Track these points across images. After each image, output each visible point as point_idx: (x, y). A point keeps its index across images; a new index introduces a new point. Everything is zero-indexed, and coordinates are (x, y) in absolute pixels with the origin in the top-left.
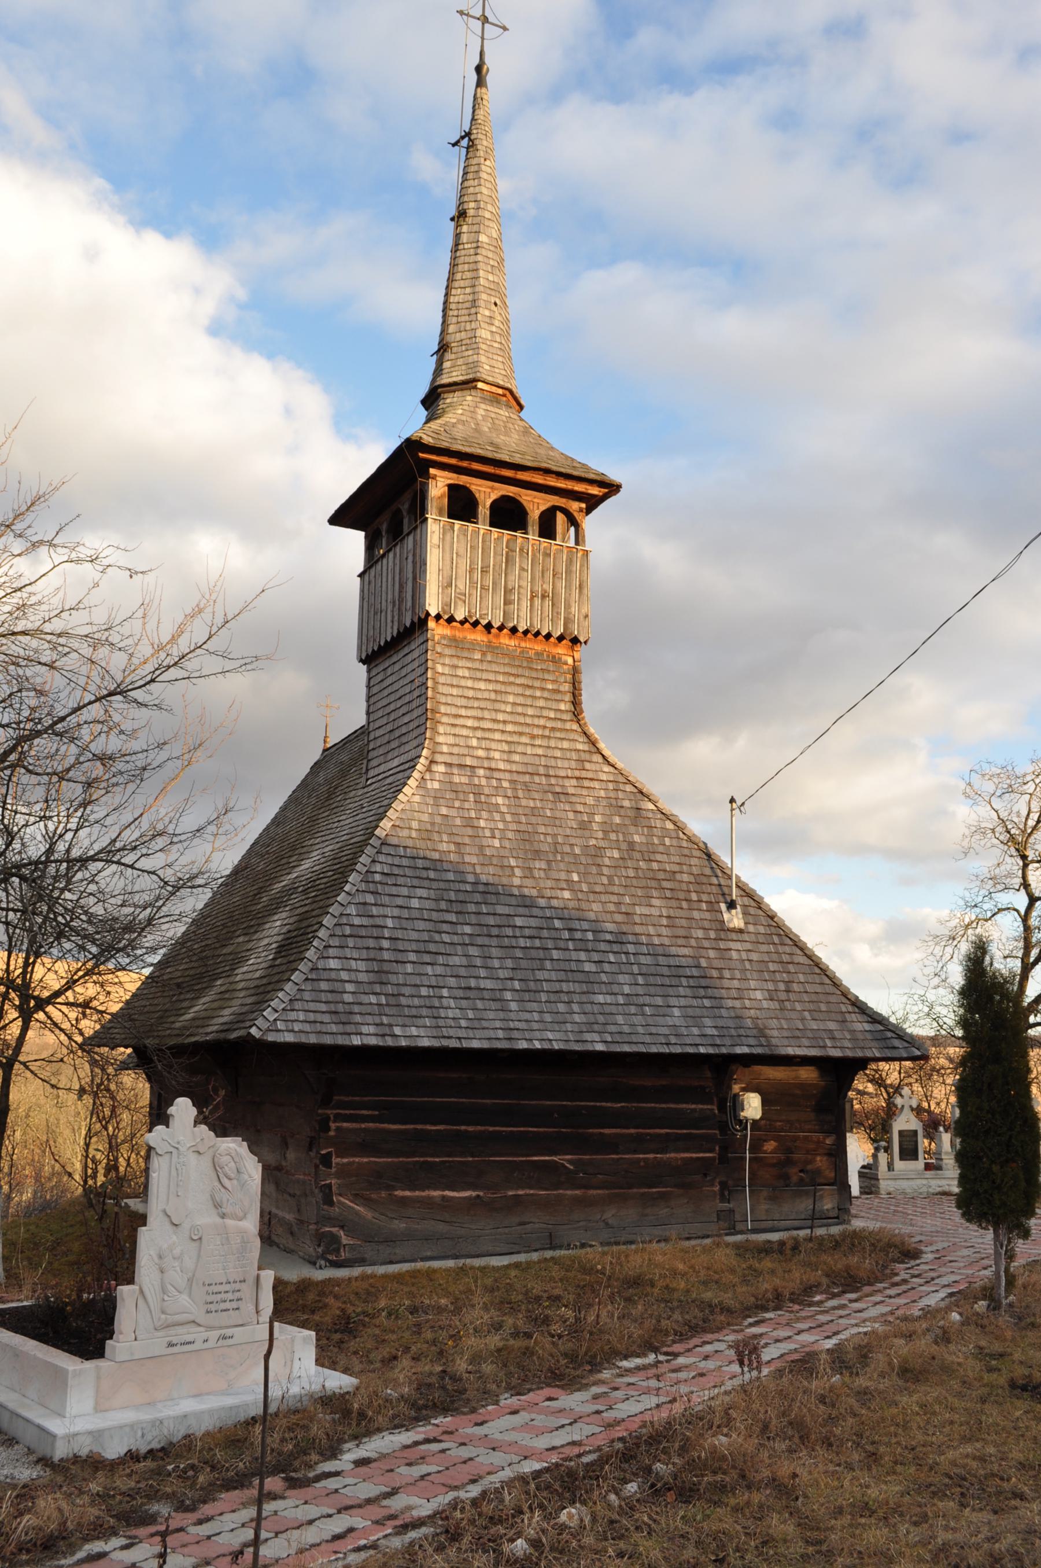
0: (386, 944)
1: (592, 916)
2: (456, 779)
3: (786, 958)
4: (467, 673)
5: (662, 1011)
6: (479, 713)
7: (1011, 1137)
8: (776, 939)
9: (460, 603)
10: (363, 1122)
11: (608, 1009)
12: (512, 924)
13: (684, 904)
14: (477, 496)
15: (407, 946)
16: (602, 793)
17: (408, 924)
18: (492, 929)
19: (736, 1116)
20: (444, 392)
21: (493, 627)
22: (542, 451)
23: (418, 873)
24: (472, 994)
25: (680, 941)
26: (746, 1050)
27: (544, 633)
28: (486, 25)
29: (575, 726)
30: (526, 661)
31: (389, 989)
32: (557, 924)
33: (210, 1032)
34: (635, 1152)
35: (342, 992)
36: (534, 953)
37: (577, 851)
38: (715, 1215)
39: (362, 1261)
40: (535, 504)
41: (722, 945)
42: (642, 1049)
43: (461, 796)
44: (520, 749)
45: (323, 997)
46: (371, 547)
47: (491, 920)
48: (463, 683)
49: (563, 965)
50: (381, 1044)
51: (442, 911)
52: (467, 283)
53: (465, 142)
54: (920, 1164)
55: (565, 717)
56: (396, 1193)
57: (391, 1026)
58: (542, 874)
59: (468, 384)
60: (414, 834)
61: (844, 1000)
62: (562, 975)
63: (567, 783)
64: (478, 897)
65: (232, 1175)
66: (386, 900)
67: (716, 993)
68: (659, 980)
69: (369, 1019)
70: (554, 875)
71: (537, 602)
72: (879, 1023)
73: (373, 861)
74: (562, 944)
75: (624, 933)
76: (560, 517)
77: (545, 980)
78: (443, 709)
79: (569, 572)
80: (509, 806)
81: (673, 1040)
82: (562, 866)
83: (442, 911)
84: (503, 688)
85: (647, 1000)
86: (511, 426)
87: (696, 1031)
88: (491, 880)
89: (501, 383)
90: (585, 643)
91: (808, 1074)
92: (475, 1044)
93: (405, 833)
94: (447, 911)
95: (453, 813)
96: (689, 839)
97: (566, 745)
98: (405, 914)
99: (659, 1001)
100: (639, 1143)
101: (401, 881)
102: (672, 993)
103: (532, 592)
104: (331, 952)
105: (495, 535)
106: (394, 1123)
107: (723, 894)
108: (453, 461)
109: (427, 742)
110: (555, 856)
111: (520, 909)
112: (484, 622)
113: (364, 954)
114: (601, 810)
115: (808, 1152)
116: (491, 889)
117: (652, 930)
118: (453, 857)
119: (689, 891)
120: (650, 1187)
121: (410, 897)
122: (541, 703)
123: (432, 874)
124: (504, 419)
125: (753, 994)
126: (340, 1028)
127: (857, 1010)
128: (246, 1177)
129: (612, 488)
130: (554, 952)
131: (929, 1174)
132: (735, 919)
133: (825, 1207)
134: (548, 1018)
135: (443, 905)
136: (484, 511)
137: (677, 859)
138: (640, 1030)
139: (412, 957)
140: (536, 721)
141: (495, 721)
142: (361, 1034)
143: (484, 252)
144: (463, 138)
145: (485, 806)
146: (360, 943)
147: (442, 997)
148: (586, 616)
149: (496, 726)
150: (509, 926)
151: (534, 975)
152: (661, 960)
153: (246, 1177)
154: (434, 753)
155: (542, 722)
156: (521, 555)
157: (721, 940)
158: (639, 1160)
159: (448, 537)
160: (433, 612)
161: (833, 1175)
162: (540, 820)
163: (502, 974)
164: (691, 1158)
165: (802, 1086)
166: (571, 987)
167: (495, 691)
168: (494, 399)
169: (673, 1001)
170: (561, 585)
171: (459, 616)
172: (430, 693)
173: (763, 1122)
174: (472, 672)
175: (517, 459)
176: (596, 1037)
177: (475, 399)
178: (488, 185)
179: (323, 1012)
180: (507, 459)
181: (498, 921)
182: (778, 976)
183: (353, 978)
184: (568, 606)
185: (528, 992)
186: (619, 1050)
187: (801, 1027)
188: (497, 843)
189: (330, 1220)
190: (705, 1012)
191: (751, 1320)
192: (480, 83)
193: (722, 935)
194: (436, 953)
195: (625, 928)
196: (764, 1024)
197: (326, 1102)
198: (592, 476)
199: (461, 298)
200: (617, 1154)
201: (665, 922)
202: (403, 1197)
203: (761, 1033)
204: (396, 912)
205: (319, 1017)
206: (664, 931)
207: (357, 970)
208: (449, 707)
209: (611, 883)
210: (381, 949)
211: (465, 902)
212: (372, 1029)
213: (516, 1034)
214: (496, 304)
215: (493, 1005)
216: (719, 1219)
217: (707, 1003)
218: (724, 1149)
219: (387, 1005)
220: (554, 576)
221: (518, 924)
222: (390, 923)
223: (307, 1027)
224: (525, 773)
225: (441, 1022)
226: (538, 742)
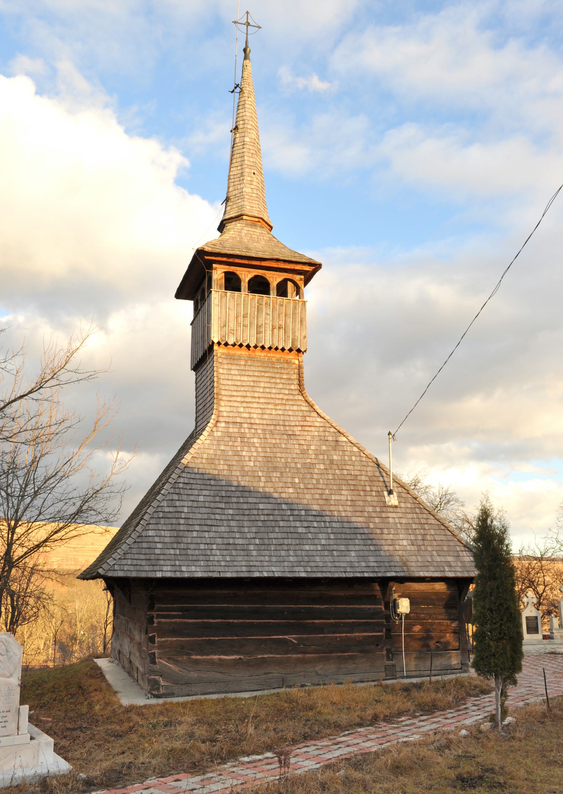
0: (182, 521)
1: (305, 502)
2: (231, 430)
3: (423, 521)
4: (236, 372)
5: (343, 553)
6: (244, 394)
7: (501, 625)
8: (418, 511)
9: (231, 335)
10: (173, 618)
11: (310, 553)
12: (257, 508)
13: (362, 493)
14: (240, 276)
15: (195, 522)
16: (316, 434)
17: (197, 510)
18: (245, 511)
19: (395, 612)
20: (227, 223)
21: (250, 347)
22: (277, 250)
23: (204, 482)
24: (230, 547)
25: (358, 514)
26: (393, 574)
27: (280, 348)
28: (249, 27)
29: (300, 397)
30: (271, 364)
31: (182, 546)
32: (284, 507)
34: (334, 633)
35: (154, 549)
36: (269, 524)
37: (299, 466)
38: (384, 668)
39: (172, 695)
40: (274, 279)
41: (384, 515)
43: (233, 439)
44: (268, 412)
45: (143, 551)
47: (245, 506)
48: (234, 378)
49: (285, 530)
50: (173, 576)
51: (217, 502)
52: (239, 164)
53: (238, 90)
54: (539, 636)
55: (294, 393)
56: (192, 657)
57: (180, 566)
58: (277, 479)
59: (239, 217)
60: (204, 461)
61: (459, 544)
62: (285, 535)
63: (295, 429)
64: (238, 494)
65: (3, 653)
66: (185, 497)
67: (378, 542)
68: (343, 536)
69: (168, 563)
70: (284, 480)
71: (276, 331)
73: (179, 477)
74: (286, 518)
75: (324, 511)
76: (290, 284)
77: (274, 538)
78: (223, 392)
79: (294, 314)
80: (260, 443)
81: (349, 569)
82: (289, 475)
83: (217, 502)
84: (258, 379)
85: (335, 547)
86: (262, 237)
87: (363, 564)
88: (247, 484)
89: (256, 215)
90: (305, 351)
91: (440, 587)
92: (229, 575)
93: (199, 461)
94: (220, 502)
95: (228, 448)
96: (367, 456)
97: (295, 408)
98: (195, 504)
99: (343, 548)
100: (336, 628)
101: (194, 487)
102: (351, 543)
103: (273, 326)
104: (151, 527)
105: (279, 300)
106: (190, 619)
107: (386, 487)
108: (225, 259)
109: (214, 411)
110: (286, 469)
111: (263, 499)
112: (245, 344)
113: (169, 527)
114: (315, 443)
115: (441, 631)
116: (246, 489)
117: (341, 508)
118: (225, 473)
119: (365, 486)
120: (343, 653)
121: (198, 495)
122: (281, 386)
123: (212, 482)
124: (258, 234)
125: (401, 542)
126: (151, 568)
127: (467, 549)
128: (12, 654)
129: (317, 267)
130: (281, 522)
131: (546, 641)
132: (393, 500)
133: (453, 663)
134: (274, 559)
135: (218, 499)
136: (244, 285)
137: (359, 468)
139: (197, 528)
140: (277, 396)
141: (253, 397)
142: (162, 571)
143: (247, 146)
144: (236, 88)
145: (246, 444)
146: (167, 521)
147: (213, 549)
148: (305, 337)
149: (254, 400)
150: (255, 509)
151: (268, 535)
152: (346, 525)
153: (12, 654)
154: (218, 416)
155: (281, 396)
156: (266, 307)
157: (383, 512)
158: (337, 637)
159: (224, 300)
160: (216, 341)
161: (457, 644)
162: (278, 450)
163: (249, 536)
164: (369, 636)
165: (436, 594)
166: (290, 541)
167: (254, 381)
168: (253, 224)
169: (351, 548)
170: (290, 320)
171: (231, 342)
172: (215, 384)
173: (412, 615)
174: (239, 371)
175: (260, 255)
176: (302, 569)
177: (242, 225)
178: (250, 111)
179: (142, 560)
180: (254, 255)
181: (249, 506)
183: (162, 540)
184: (294, 332)
185: (263, 546)
186: (314, 576)
187: (430, 560)
189: (153, 672)
190: (370, 553)
191: (347, 732)
193: (384, 509)
194: (211, 526)
195: (325, 508)
196: (406, 559)
197: (151, 607)
198: (304, 260)
199: (235, 173)
200: (323, 634)
201: (349, 503)
202: (196, 659)
203: (405, 564)
204: (190, 504)
205: (139, 562)
206: (348, 508)
207: (164, 536)
208: (227, 391)
209: (318, 483)
210: (179, 524)
211: (231, 497)
212: (169, 568)
213: (253, 569)
214: (254, 174)
215: (242, 553)
216: (386, 670)
217: (372, 548)
218: (389, 630)
219: (180, 555)
220: (285, 316)
221: (261, 508)
222: (186, 510)
223: (132, 568)
224: (271, 425)
225: (210, 563)
226: (279, 407)
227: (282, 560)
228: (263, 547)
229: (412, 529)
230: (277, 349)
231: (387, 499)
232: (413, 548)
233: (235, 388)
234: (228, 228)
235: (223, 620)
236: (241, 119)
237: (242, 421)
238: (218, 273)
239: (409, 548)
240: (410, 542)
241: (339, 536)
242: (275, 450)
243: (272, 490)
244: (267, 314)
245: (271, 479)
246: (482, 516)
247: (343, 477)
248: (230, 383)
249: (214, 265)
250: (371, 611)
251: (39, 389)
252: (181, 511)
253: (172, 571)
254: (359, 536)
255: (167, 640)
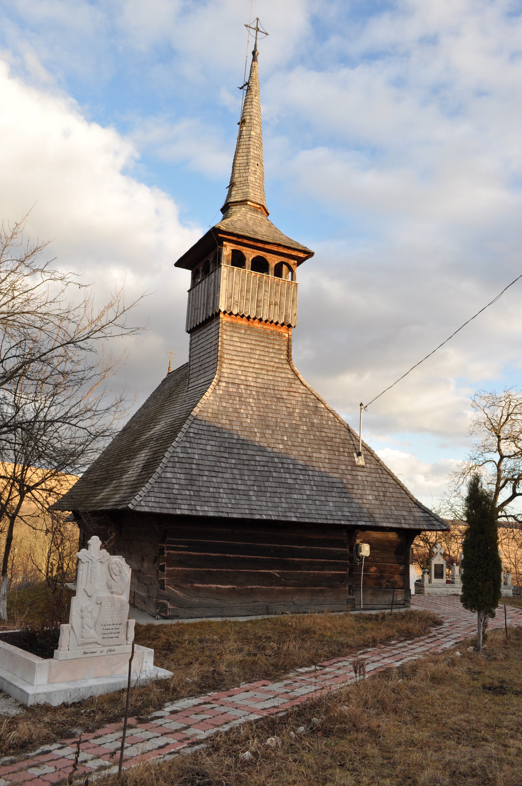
0: (194, 467)
1: (292, 457)
2: (231, 390)
4: (237, 340)
6: (242, 359)
7: (487, 569)
8: (380, 471)
9: (235, 306)
10: (180, 551)
11: (298, 501)
12: (254, 459)
13: (337, 453)
14: (245, 255)
16: (300, 399)
17: (205, 458)
18: (245, 461)
21: (250, 318)
23: (211, 433)
26: (363, 523)
28: (258, 32)
29: (288, 367)
31: (195, 488)
32: (276, 460)
33: (109, 505)
34: (309, 570)
35: (172, 489)
36: (264, 474)
37: (287, 426)
39: (177, 617)
40: (273, 260)
41: (354, 473)
42: (314, 521)
43: (233, 398)
44: (261, 376)
45: (164, 490)
46: (194, 278)
47: (245, 457)
48: (235, 344)
50: (190, 514)
52: (244, 154)
53: (246, 87)
54: (444, 581)
55: (283, 362)
56: (195, 585)
57: (195, 505)
59: (243, 202)
60: (210, 415)
61: (411, 501)
62: (277, 485)
63: (283, 393)
64: (239, 446)
66: (195, 446)
68: (323, 489)
69: (185, 502)
70: (275, 437)
71: (272, 307)
72: (427, 513)
74: (278, 470)
76: (285, 267)
78: (225, 356)
79: (288, 293)
81: (329, 517)
82: (279, 433)
85: (317, 498)
87: (340, 513)
88: (245, 438)
89: (259, 202)
90: (294, 327)
92: (235, 516)
94: (224, 452)
98: (204, 453)
99: (323, 498)
100: (311, 566)
101: (202, 437)
102: (329, 495)
103: (270, 302)
104: (168, 469)
107: (355, 449)
108: (235, 239)
109: (217, 371)
110: (276, 428)
112: (247, 315)
113: (184, 471)
115: (391, 573)
116: (245, 442)
118: (227, 426)
120: (315, 587)
121: (206, 445)
125: (367, 497)
127: (417, 506)
128: (124, 575)
129: (310, 254)
131: (448, 585)
132: (360, 461)
134: (270, 504)
135: (222, 449)
136: (248, 263)
137: (334, 431)
138: (314, 512)
139: (207, 473)
140: (269, 364)
141: (250, 362)
142: (181, 509)
144: (245, 85)
145: (244, 403)
146: (182, 465)
147: (220, 493)
148: (295, 315)
149: (250, 365)
151: (264, 484)
152: (325, 479)
153: (124, 575)
154: (220, 377)
155: (272, 364)
156: (265, 285)
159: (231, 274)
160: (223, 310)
161: (402, 584)
162: (270, 410)
163: (249, 483)
165: (390, 541)
166: (282, 490)
167: (251, 349)
168: (255, 210)
169: (330, 499)
171: (235, 313)
172: (220, 348)
173: (370, 558)
175: (265, 239)
178: (256, 108)
179: (163, 498)
180: (260, 238)
182: (380, 489)
183: (178, 482)
184: (287, 310)
185: (261, 492)
188: (249, 421)
190: (345, 505)
192: (254, 59)
193: (354, 468)
197: (163, 540)
198: (300, 248)
199: (241, 161)
200: (300, 570)
201: (327, 461)
202: (198, 587)
203: (371, 515)
204: (200, 452)
205: (161, 500)
209: (302, 442)
210: (192, 469)
214: (258, 165)
216: (347, 603)
217: (346, 500)
218: (351, 570)
219: (194, 495)
221: (257, 459)
222: (196, 457)
223: (155, 505)
225: (219, 505)
226: (270, 373)
227: (276, 506)
228: (260, 494)
229: (375, 486)
230: (272, 322)
231: (356, 459)
232: (377, 502)
233: (235, 353)
234: (233, 210)
235: (221, 555)
236: (248, 114)
237: (240, 382)
238: (227, 250)
239: (373, 502)
240: (374, 497)
241: (320, 488)
242: (267, 410)
243: (266, 445)
244: (266, 291)
245: (265, 435)
246: (474, 481)
247: (321, 438)
248: (231, 348)
249: (225, 243)
250: (339, 553)
251: (86, 338)
252: (193, 457)
253: (188, 510)
254: (335, 490)
255: (175, 569)
